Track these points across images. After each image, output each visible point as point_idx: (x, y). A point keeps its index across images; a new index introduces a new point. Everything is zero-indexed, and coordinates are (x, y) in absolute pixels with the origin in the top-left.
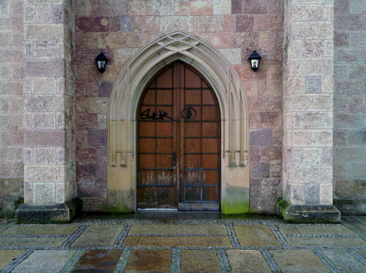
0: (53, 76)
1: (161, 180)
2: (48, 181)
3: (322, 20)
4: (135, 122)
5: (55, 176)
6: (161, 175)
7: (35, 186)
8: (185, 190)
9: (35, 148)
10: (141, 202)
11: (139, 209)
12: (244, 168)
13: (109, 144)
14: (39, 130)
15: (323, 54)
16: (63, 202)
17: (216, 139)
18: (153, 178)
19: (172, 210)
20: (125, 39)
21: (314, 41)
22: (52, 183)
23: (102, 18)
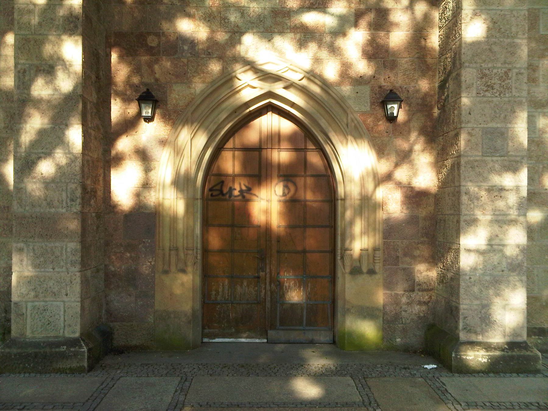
0: (63, 124)
1: (241, 294)
2: (52, 299)
3: (508, 37)
4: (199, 203)
5: (64, 291)
6: (241, 286)
7: (29, 308)
8: (278, 309)
9: (31, 244)
10: (209, 327)
11: (206, 340)
12: (374, 276)
13: (157, 237)
14: (39, 214)
15: (511, 92)
16: (77, 335)
17: (328, 229)
18: (228, 290)
19: (257, 341)
20: (186, 68)
21: (495, 71)
22: (58, 303)
23: (149, 34)
